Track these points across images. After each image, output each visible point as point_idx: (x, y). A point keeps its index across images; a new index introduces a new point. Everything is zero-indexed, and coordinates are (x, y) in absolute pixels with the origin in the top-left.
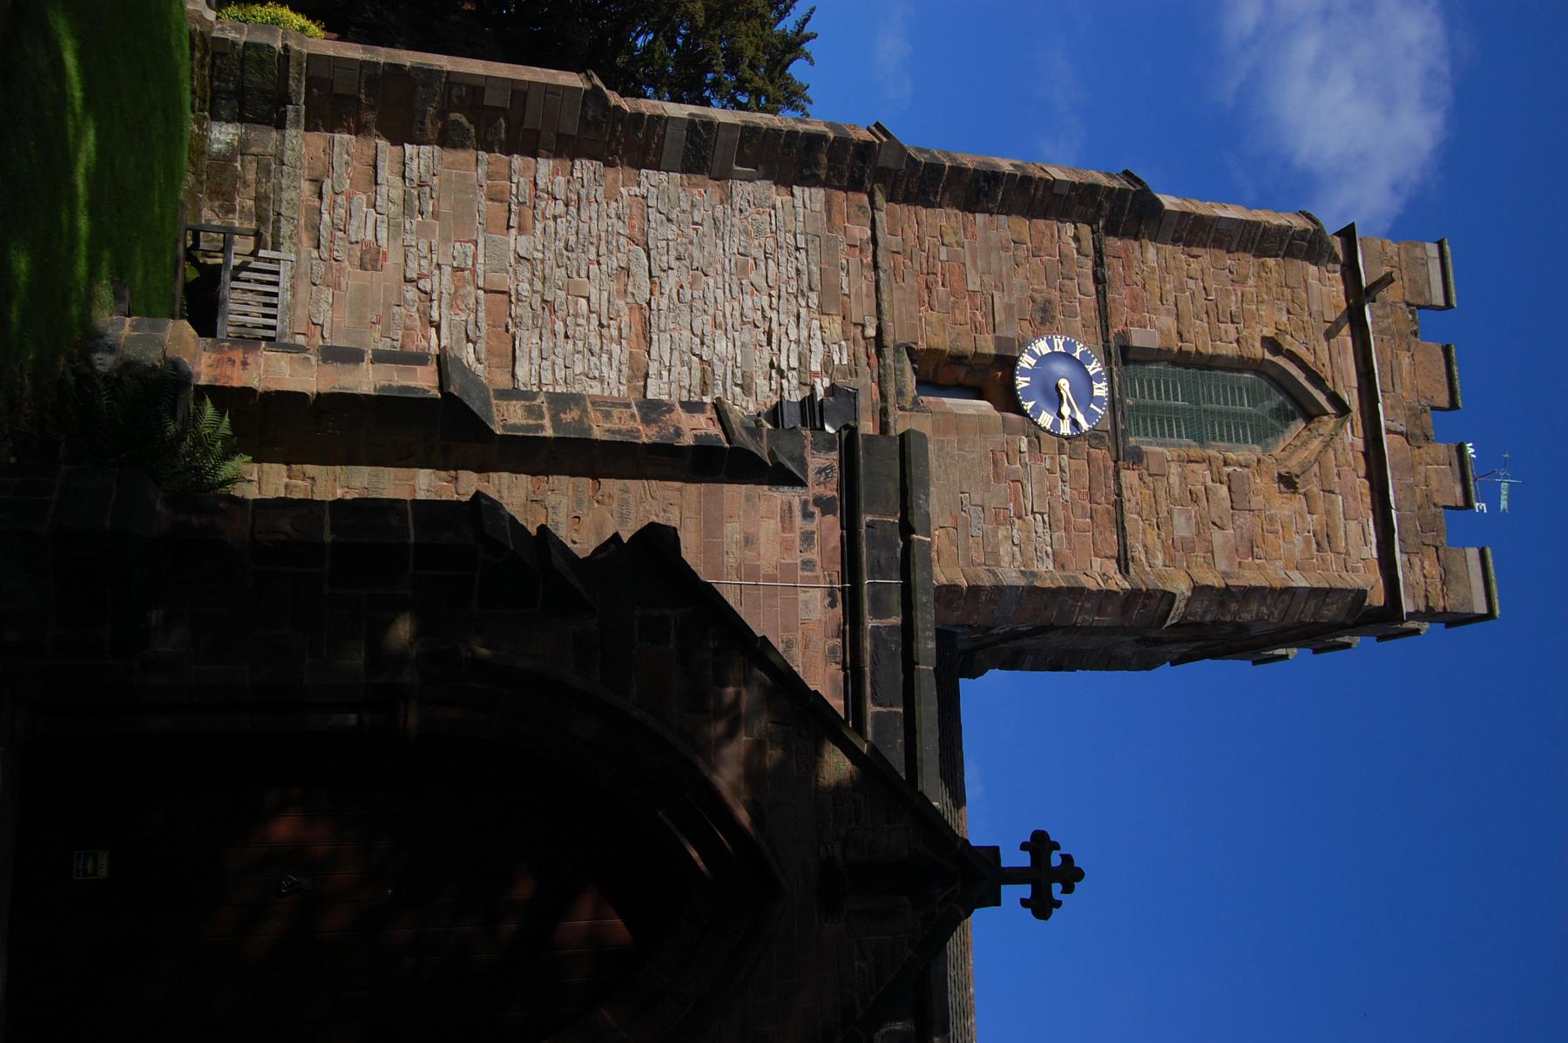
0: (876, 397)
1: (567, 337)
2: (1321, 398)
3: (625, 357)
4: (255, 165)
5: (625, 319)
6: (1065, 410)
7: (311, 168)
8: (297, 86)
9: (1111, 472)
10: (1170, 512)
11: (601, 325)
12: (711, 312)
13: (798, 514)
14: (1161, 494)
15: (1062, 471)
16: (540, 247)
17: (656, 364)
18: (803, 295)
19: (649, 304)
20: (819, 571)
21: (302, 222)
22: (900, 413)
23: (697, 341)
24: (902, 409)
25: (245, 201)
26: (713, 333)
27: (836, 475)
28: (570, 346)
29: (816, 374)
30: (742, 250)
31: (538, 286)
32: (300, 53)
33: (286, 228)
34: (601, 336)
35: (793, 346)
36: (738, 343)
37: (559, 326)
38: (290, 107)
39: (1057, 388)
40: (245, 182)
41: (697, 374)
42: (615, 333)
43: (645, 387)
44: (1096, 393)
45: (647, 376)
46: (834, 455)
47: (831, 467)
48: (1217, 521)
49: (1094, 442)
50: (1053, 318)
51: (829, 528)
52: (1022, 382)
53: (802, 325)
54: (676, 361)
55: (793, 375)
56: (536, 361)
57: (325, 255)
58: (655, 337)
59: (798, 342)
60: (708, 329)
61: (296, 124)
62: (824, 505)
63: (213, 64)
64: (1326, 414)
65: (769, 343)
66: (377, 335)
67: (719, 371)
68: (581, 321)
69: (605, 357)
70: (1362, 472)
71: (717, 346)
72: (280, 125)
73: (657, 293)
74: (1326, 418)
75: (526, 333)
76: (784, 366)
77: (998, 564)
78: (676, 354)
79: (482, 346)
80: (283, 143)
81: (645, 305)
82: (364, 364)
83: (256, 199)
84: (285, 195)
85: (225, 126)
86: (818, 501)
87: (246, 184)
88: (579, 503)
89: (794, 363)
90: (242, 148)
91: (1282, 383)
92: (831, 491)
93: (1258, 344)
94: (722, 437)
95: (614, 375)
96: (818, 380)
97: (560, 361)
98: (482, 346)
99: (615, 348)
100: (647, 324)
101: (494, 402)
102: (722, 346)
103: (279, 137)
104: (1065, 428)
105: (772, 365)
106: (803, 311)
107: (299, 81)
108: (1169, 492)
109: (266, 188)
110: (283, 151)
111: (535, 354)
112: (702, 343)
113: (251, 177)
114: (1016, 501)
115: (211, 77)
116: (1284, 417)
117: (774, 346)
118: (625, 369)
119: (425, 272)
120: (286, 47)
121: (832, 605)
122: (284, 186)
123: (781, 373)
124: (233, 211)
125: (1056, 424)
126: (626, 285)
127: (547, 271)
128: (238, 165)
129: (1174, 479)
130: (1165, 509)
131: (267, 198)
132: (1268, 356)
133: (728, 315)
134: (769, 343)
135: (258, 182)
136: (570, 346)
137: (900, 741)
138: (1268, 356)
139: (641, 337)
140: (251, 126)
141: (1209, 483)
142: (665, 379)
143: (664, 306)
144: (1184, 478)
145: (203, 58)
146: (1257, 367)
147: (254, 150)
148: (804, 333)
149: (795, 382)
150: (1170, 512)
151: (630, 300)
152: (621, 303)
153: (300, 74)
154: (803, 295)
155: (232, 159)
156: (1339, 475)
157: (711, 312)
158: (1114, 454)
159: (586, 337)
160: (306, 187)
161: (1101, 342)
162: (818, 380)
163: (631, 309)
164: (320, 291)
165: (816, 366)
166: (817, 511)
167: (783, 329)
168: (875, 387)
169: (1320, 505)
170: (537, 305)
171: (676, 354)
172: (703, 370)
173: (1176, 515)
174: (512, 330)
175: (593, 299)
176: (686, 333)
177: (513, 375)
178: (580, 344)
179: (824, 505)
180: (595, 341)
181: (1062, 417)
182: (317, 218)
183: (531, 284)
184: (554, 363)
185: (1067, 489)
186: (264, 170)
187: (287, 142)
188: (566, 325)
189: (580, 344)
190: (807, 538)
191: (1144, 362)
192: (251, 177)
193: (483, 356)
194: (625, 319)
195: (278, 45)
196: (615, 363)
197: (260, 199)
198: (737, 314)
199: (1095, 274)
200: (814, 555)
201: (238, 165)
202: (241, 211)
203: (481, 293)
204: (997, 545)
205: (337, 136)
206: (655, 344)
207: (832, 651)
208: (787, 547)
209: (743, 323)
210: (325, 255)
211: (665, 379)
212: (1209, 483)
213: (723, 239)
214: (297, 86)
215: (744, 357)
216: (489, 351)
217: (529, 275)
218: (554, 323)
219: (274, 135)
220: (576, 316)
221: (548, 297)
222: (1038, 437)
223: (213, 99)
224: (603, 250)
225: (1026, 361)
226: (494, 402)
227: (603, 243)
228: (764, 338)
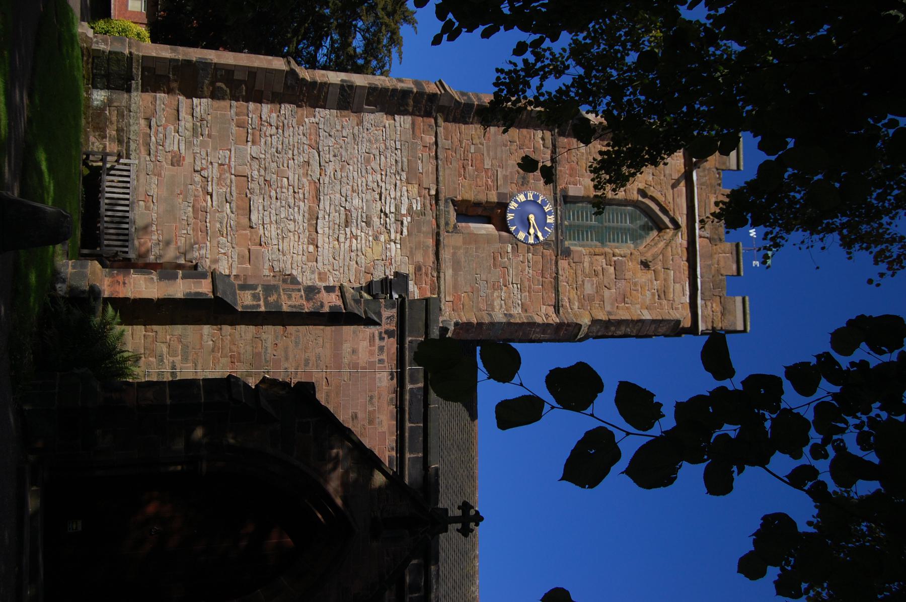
0: (435, 226)
1: (277, 199)
2: (666, 220)
3: (306, 209)
4: (116, 112)
5: (307, 188)
6: (532, 231)
7: (145, 113)
8: (137, 71)
9: (553, 262)
10: (583, 281)
11: (294, 192)
12: (351, 184)
13: (377, 338)
14: (579, 272)
15: (528, 261)
16: (263, 152)
17: (322, 212)
18: (398, 174)
19: (319, 180)
20: (386, 364)
21: (141, 141)
22: (446, 234)
23: (343, 199)
24: (447, 232)
25: (111, 132)
26: (352, 195)
27: (395, 320)
28: (279, 203)
29: (404, 215)
30: (367, 151)
31: (262, 172)
32: (138, 56)
33: (133, 146)
34: (294, 198)
35: (393, 200)
36: (364, 200)
37: (273, 193)
38: (133, 82)
39: (528, 219)
40: (111, 122)
41: (343, 217)
42: (301, 196)
43: (317, 224)
44: (548, 221)
45: (317, 218)
46: (395, 310)
47: (393, 316)
48: (607, 285)
49: (546, 247)
50: (528, 182)
51: (391, 344)
52: (510, 216)
53: (397, 190)
54: (332, 210)
55: (392, 216)
56: (261, 211)
57: (153, 159)
58: (322, 198)
59: (395, 199)
60: (349, 193)
61: (137, 89)
62: (390, 334)
63: (93, 62)
64: (668, 228)
65: (380, 199)
66: (180, 201)
67: (354, 215)
68: (284, 190)
69: (296, 209)
70: (685, 258)
71: (354, 202)
72: (129, 90)
73: (323, 175)
74: (668, 230)
75: (256, 198)
76: (388, 211)
77: (493, 310)
78: (332, 207)
79: (234, 205)
80: (130, 100)
81: (317, 181)
82: (178, 280)
83: (118, 131)
84: (132, 128)
85: (100, 91)
86: (386, 332)
87: (111, 123)
88: (277, 337)
89: (393, 210)
90: (109, 103)
91: (647, 212)
92: (393, 327)
93: (635, 192)
94: (342, 306)
95: (301, 218)
96: (405, 218)
97: (273, 212)
98: (234, 205)
99: (302, 204)
100: (318, 191)
101: (238, 292)
102: (356, 202)
103: (128, 97)
104: (531, 240)
105: (381, 211)
106: (398, 182)
107: (138, 69)
108: (583, 271)
109: (123, 124)
110: (130, 105)
111: (261, 208)
112: (346, 200)
113: (114, 119)
114: (504, 278)
115: (92, 68)
116: (647, 229)
117: (383, 201)
118: (306, 215)
119: (204, 167)
120: (131, 53)
121: (392, 379)
122: (131, 123)
123: (386, 215)
124: (105, 137)
125: (526, 238)
126: (307, 170)
127: (267, 164)
128: (107, 112)
129: (586, 264)
130: (580, 279)
131: (123, 130)
132: (640, 198)
133: (360, 186)
134: (380, 199)
135: (118, 122)
136: (279, 203)
137: (421, 439)
138: (640, 198)
139: (315, 199)
140: (113, 91)
141: (605, 266)
142: (327, 220)
143: (327, 181)
144: (591, 263)
145: (88, 59)
146: (635, 204)
147: (115, 104)
148: (399, 194)
149: (393, 220)
150: (583, 281)
151: (309, 178)
152: (305, 180)
153: (138, 65)
154: (398, 174)
155: (104, 110)
156: (672, 260)
157: (351, 184)
158: (556, 253)
159: (287, 198)
160: (143, 122)
161: (552, 194)
162: (405, 218)
163: (310, 183)
164: (151, 178)
165: (404, 211)
166: (386, 336)
167: (388, 192)
168: (434, 221)
169: (662, 276)
170: (262, 183)
171: (332, 207)
172: (346, 215)
173: (586, 283)
174: (249, 195)
175: (290, 178)
176: (338, 195)
177: (250, 219)
178: (284, 202)
179: (390, 334)
180: (291, 201)
181: (530, 234)
182: (149, 139)
183: (259, 172)
184: (270, 213)
185: (531, 271)
186: (121, 115)
187: (132, 99)
188: (276, 193)
189: (284, 202)
190: (381, 349)
191: (575, 203)
192: (114, 119)
193: (234, 210)
194: (307, 188)
195: (127, 52)
196: (301, 212)
197: (119, 130)
198: (364, 184)
199: (551, 157)
200: (384, 357)
201: (107, 112)
202: (110, 137)
203: (233, 176)
204: (493, 301)
205: (158, 95)
206: (322, 202)
207: (391, 399)
208: (371, 353)
209: (367, 189)
210: (153, 159)
211: (327, 220)
212: (605, 266)
213: (358, 145)
214: (137, 71)
215: (368, 207)
216: (237, 207)
217: (258, 167)
218: (270, 192)
219: (126, 95)
220: (282, 188)
221: (268, 179)
222: (517, 245)
223: (93, 79)
224: (296, 152)
225: (513, 205)
226: (238, 292)
227: (296, 149)
228: (377, 197)
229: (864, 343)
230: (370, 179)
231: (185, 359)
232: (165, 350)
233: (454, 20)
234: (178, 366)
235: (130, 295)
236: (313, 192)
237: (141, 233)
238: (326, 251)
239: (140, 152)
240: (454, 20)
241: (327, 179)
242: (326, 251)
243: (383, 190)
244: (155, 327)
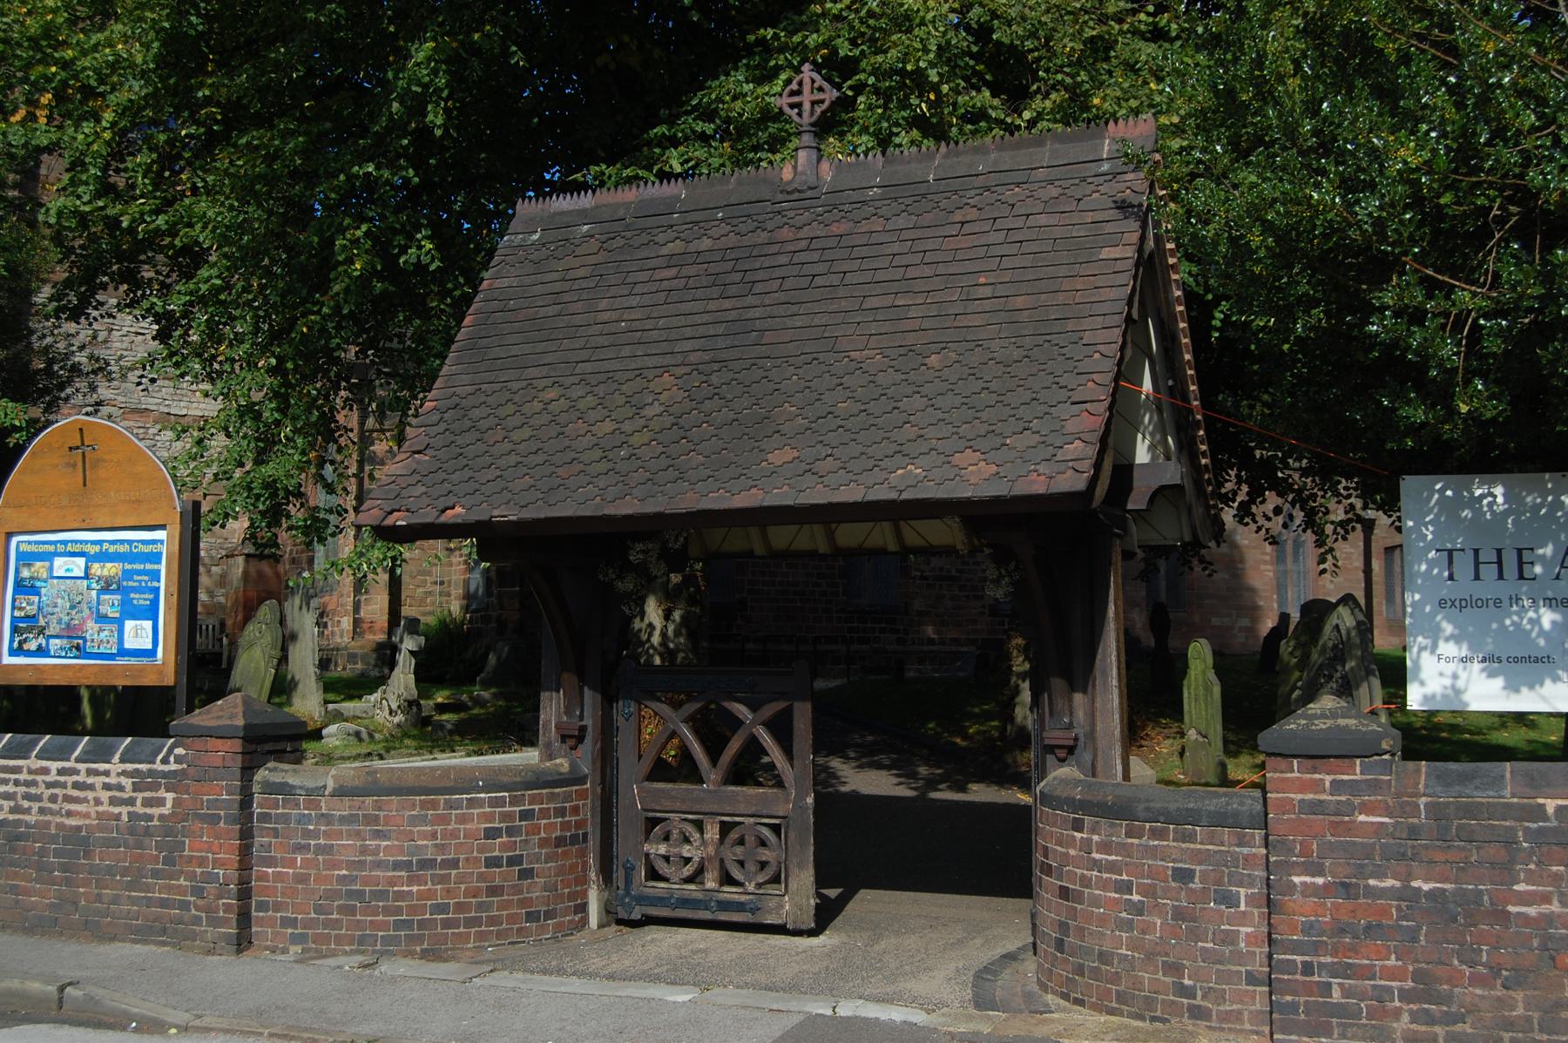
5: (132, 423)
42: (142, 431)
45: (169, 414)
143: (124, 399)
194: (132, 423)
228: (140, 338)
229: (1203, 641)
230: (118, 345)
231: (429, 573)
232: (421, 590)
233: (1307, 958)
234: (434, 579)
235: (386, 617)
236: (136, 417)
237: (252, 594)
238: (209, 407)
239: (1111, 1012)
240: (1307, 958)
241: (120, 398)
242: (209, 407)
243: (133, 330)
244: (403, 598)
